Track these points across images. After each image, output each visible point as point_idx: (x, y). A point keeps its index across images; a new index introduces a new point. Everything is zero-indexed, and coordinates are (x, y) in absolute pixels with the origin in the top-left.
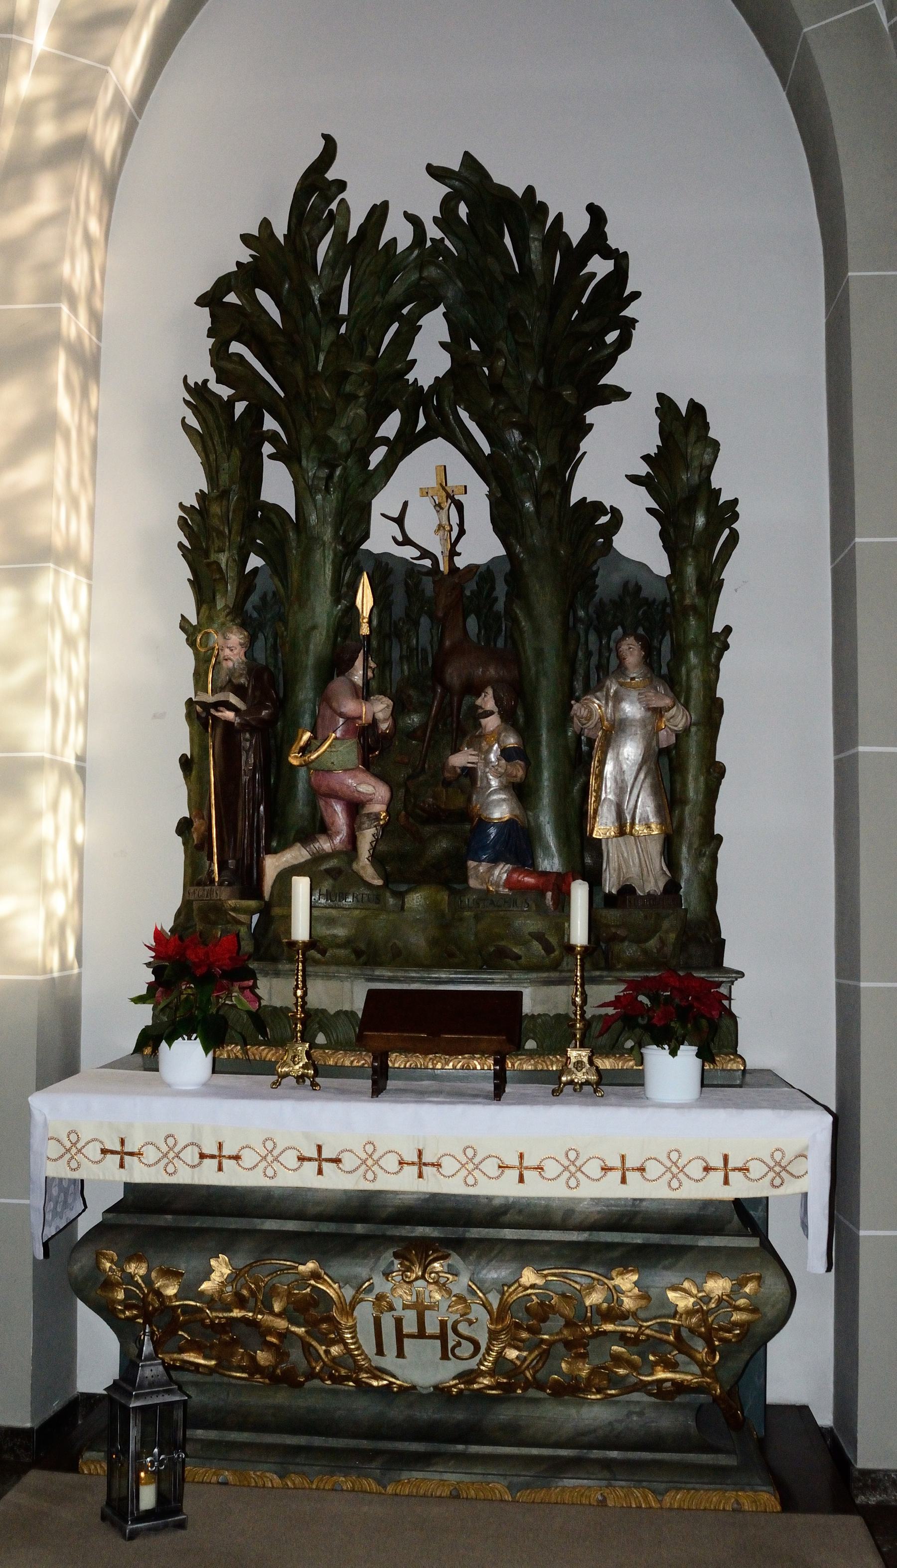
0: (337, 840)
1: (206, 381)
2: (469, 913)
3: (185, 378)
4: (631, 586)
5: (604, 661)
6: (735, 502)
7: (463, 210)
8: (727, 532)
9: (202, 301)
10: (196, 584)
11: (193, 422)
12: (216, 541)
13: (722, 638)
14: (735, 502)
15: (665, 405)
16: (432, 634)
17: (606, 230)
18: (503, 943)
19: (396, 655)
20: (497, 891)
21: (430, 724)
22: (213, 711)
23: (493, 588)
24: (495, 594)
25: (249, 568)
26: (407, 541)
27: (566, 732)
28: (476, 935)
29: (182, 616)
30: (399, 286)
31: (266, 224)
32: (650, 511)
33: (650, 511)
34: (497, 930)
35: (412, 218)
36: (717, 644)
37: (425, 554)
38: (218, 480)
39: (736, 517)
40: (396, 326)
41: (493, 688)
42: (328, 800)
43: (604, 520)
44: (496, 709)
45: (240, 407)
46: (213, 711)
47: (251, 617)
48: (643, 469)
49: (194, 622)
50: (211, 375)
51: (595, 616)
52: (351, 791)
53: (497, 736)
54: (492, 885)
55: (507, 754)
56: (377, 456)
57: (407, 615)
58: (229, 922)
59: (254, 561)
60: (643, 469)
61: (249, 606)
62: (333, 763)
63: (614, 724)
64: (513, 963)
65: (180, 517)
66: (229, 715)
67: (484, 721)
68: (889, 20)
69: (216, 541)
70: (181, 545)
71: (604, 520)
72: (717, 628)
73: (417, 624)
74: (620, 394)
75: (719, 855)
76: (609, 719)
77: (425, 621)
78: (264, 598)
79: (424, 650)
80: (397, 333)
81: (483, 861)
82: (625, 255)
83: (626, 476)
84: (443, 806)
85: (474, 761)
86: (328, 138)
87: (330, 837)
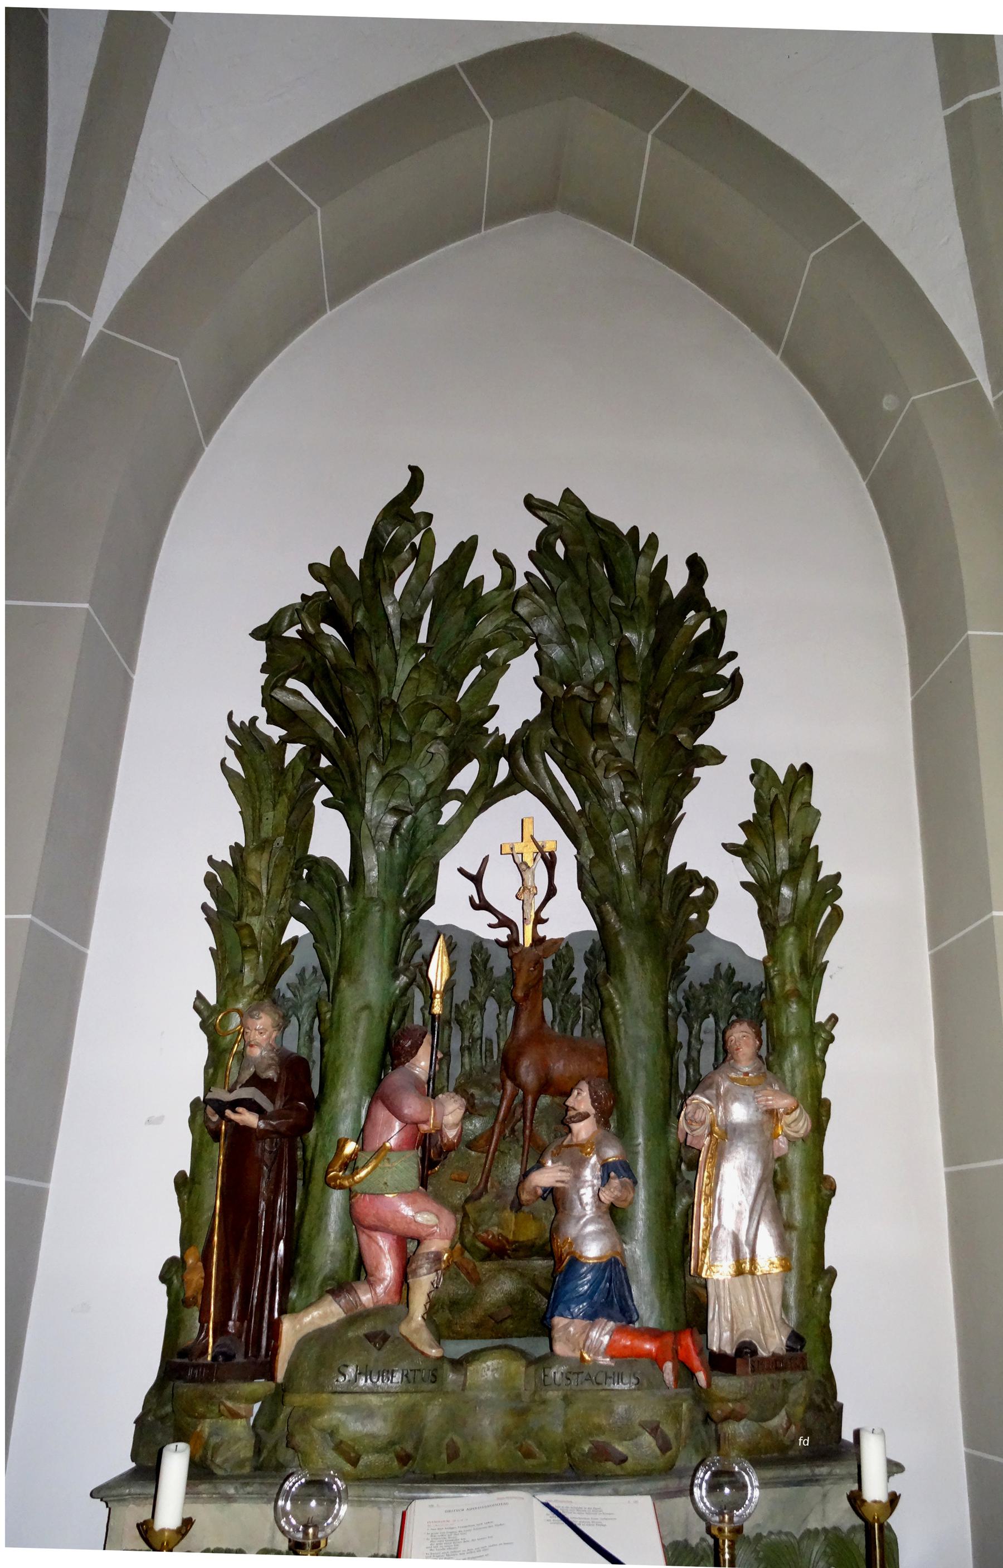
0: (380, 1289)
1: (254, 720)
2: (556, 1393)
3: (230, 715)
4: (723, 969)
5: (694, 1054)
6: (838, 876)
7: (560, 549)
8: (829, 909)
9: (257, 634)
10: (220, 956)
11: (235, 764)
12: (251, 901)
13: (828, 1028)
14: (838, 876)
15: (760, 771)
16: (499, 1020)
17: (704, 587)
18: (602, 1438)
19: (455, 1045)
20: (595, 1361)
21: (497, 1130)
22: (228, 1113)
23: (571, 969)
24: (573, 975)
25: (287, 937)
26: (481, 905)
27: (667, 1140)
28: (565, 1425)
29: (198, 993)
30: (485, 627)
31: (339, 554)
32: (745, 885)
33: (745, 885)
34: (596, 1420)
35: (502, 560)
36: (823, 1035)
37: (504, 922)
38: (259, 831)
39: (838, 893)
40: (477, 670)
41: (589, 1083)
42: (374, 1234)
43: (698, 892)
44: (592, 1111)
45: (293, 750)
46: (228, 1113)
47: (283, 996)
48: (740, 838)
49: (212, 999)
50: (262, 714)
51: (683, 1002)
52: (406, 1222)
53: (595, 1145)
54: (588, 1353)
55: (607, 1170)
56: (450, 809)
57: (472, 997)
58: (221, 1414)
59: (295, 929)
60: (740, 838)
61: (282, 984)
62: (386, 1183)
63: (726, 1130)
64: (618, 1470)
65: (208, 874)
66: (249, 1119)
67: (576, 1127)
68: (994, 395)
69: (251, 901)
70: (205, 907)
71: (698, 892)
72: (821, 1017)
73: (482, 1008)
74: (716, 757)
75: (832, 1295)
76: (720, 1124)
77: (491, 1005)
78: (301, 975)
79: (489, 1041)
80: (479, 677)
81: (577, 1317)
82: (723, 613)
83: (724, 845)
84: (511, 1237)
85: (564, 1179)
86: (416, 472)
87: (372, 1285)
